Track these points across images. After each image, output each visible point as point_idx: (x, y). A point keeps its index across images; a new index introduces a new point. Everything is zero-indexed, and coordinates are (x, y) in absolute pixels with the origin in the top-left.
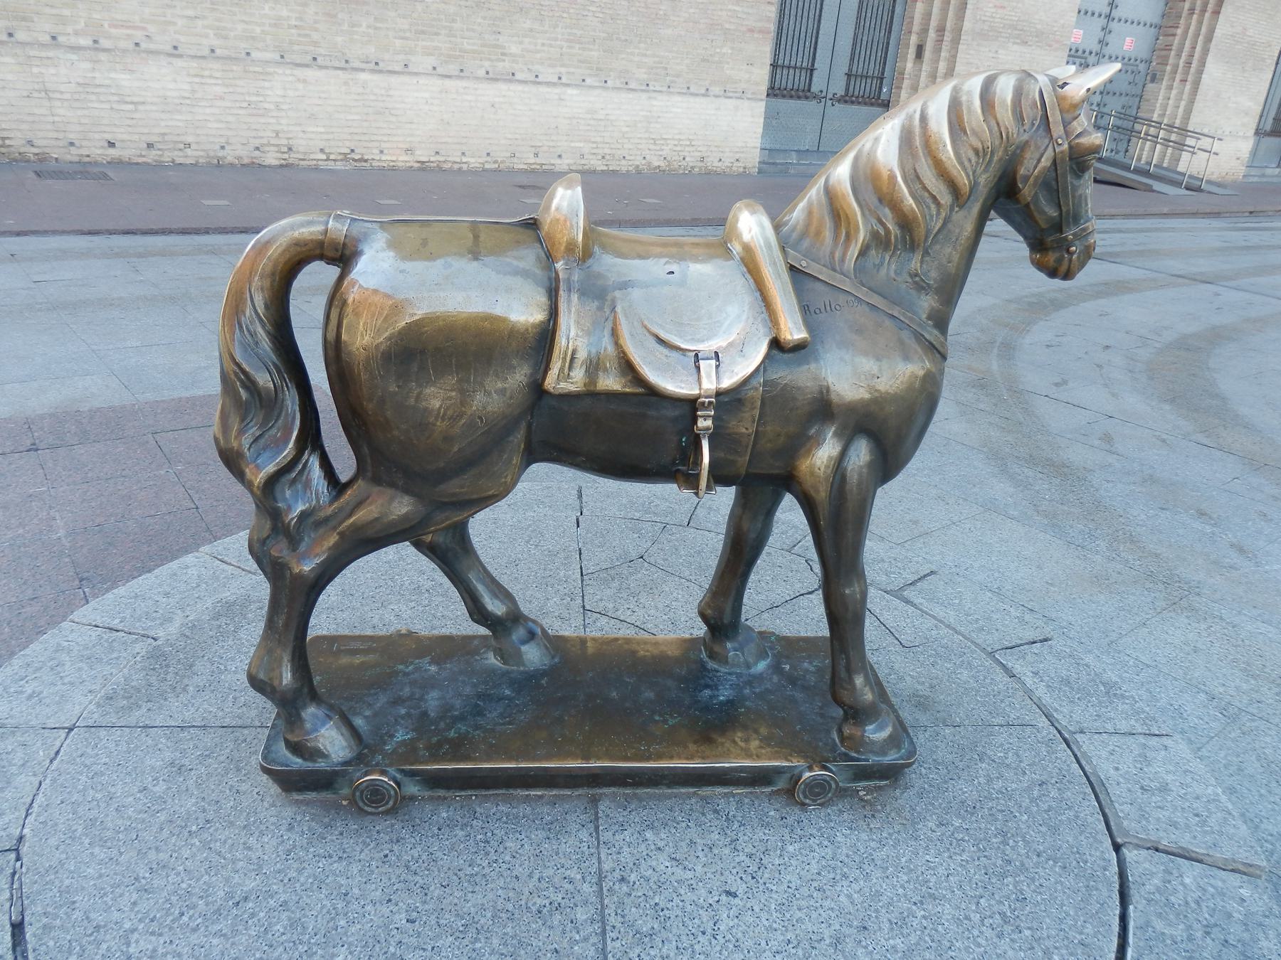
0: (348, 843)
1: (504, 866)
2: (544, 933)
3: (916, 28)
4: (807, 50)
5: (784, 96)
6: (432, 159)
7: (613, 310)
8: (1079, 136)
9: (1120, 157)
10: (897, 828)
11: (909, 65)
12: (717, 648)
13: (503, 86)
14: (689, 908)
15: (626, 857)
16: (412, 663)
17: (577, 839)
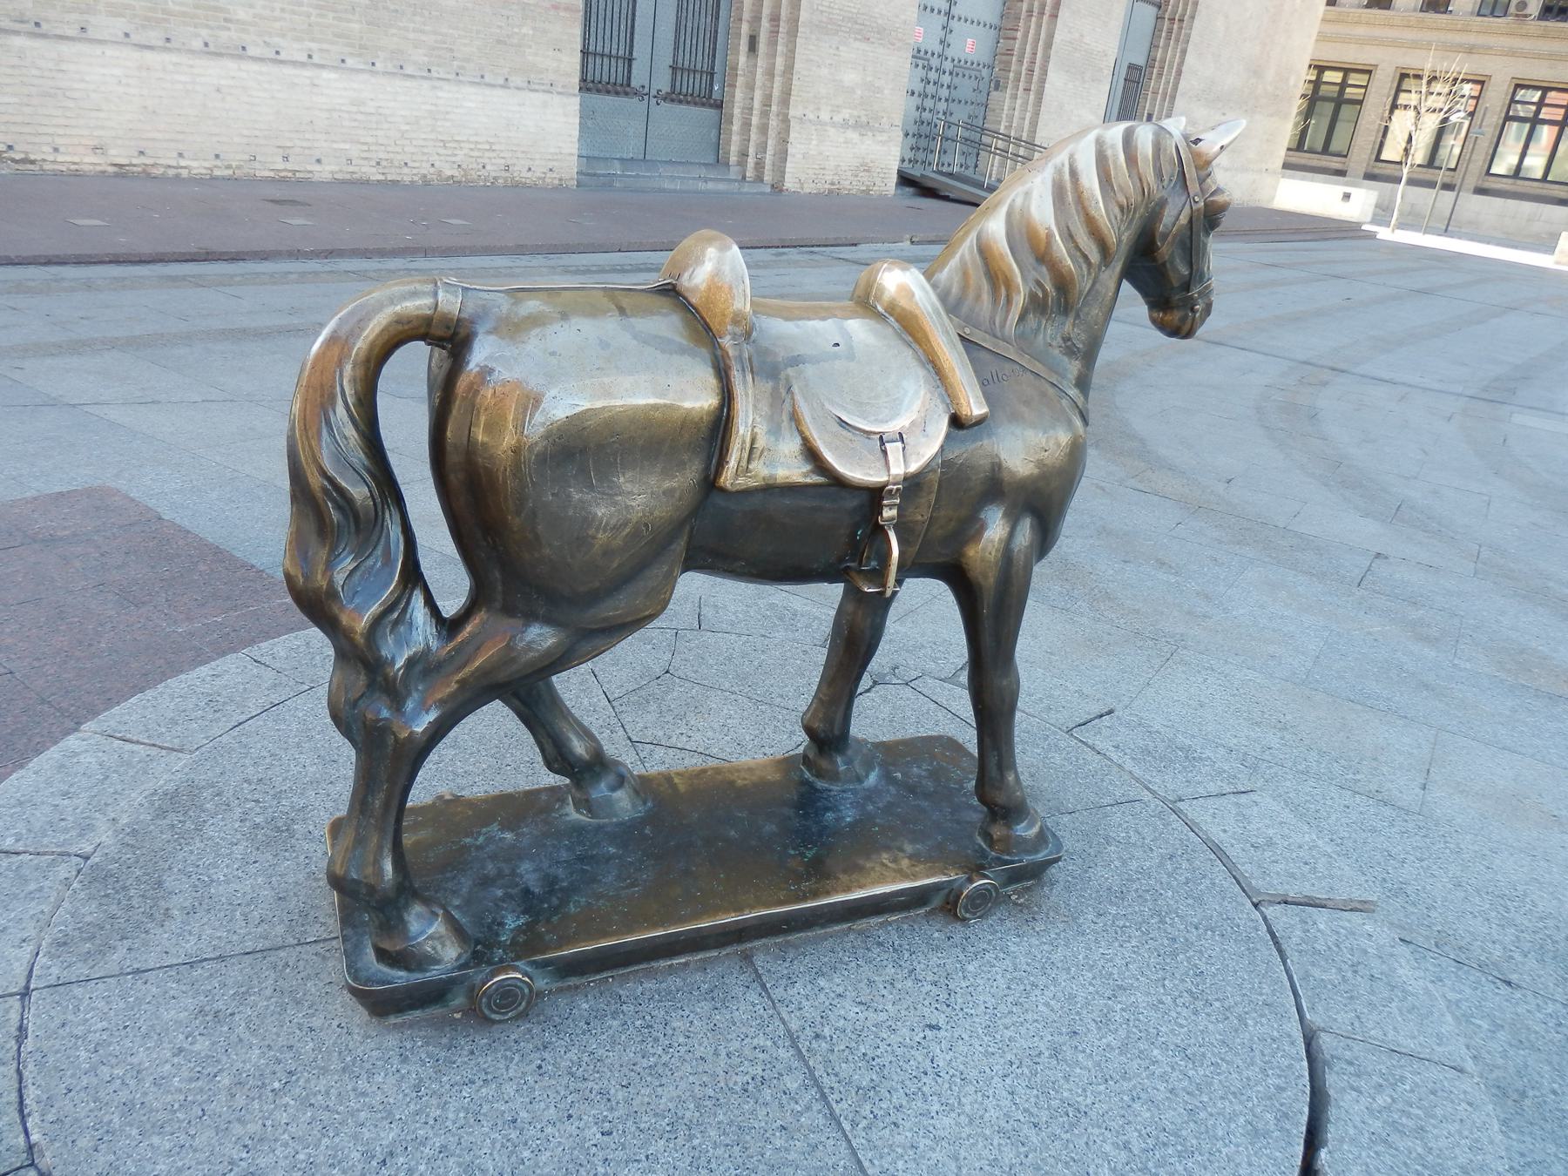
0: (486, 1061)
1: (683, 1049)
2: (762, 1112)
3: (746, 15)
4: (622, 35)
5: (598, 91)
6: (135, 161)
7: (789, 390)
8: (1213, 194)
9: (969, 173)
10: (1061, 926)
11: (742, 59)
12: (824, 764)
13: (231, 65)
14: (899, 1051)
15: (809, 1011)
16: (479, 833)
17: (747, 1004)
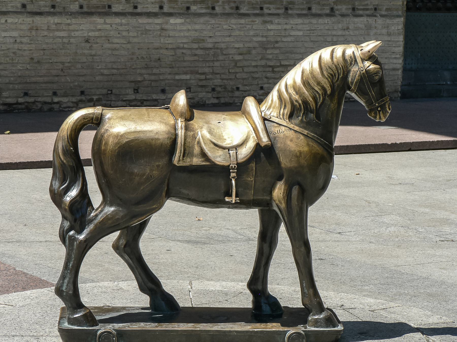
6: (21, 100)
